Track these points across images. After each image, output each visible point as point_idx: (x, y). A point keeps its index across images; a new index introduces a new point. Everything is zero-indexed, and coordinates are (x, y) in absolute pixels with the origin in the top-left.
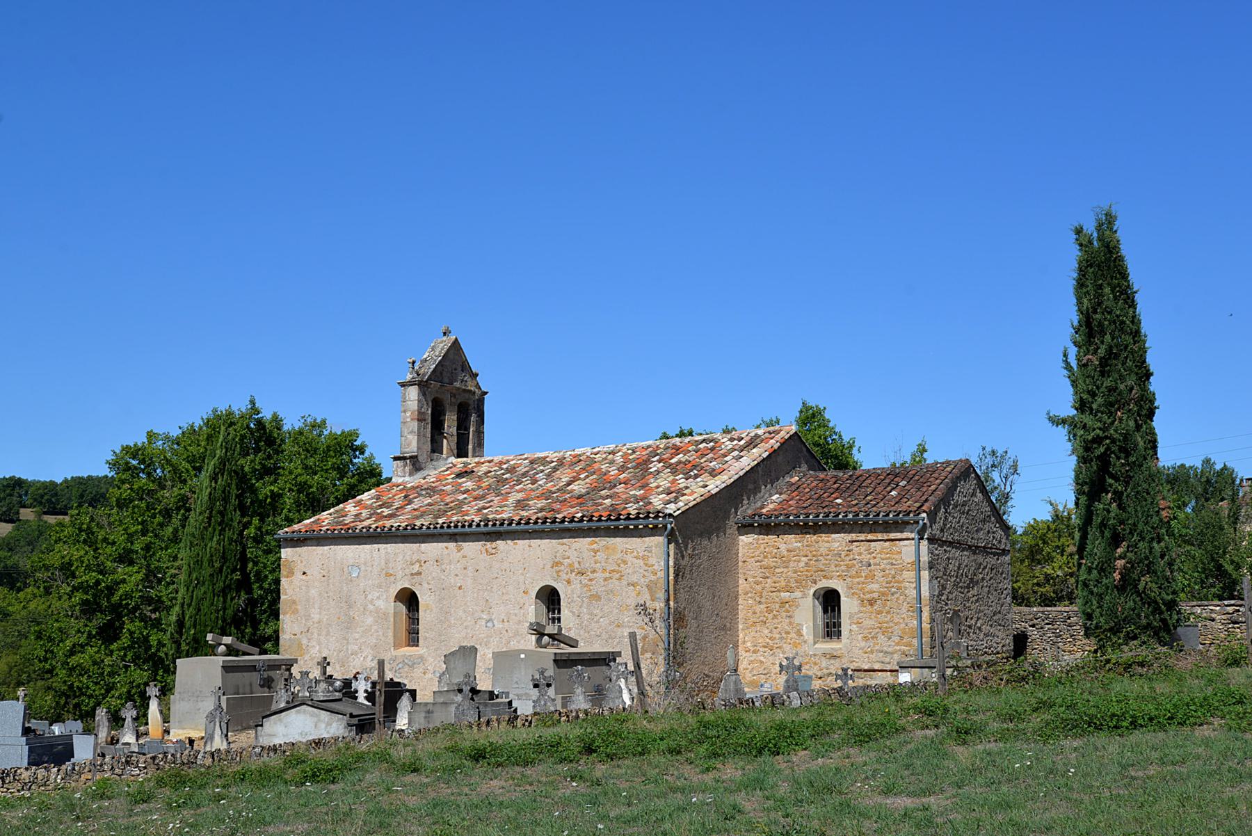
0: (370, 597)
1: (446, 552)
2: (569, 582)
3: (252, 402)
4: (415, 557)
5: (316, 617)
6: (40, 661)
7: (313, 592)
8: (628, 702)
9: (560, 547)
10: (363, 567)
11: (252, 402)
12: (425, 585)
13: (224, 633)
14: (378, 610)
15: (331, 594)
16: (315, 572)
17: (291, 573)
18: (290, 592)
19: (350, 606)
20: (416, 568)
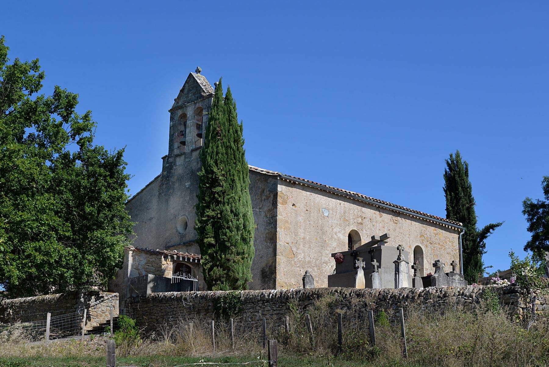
0: (335, 230)
1: (374, 216)
2: (426, 246)
3: (120, 155)
4: (360, 214)
5: (302, 235)
6: (241, 322)
7: (300, 219)
8: (49, 315)
9: (423, 228)
10: (331, 212)
11: (120, 155)
12: (364, 231)
13: (525, 276)
14: (339, 239)
15: (312, 223)
16: (301, 205)
17: (285, 202)
18: (284, 215)
19: (323, 233)
20: (360, 220)
